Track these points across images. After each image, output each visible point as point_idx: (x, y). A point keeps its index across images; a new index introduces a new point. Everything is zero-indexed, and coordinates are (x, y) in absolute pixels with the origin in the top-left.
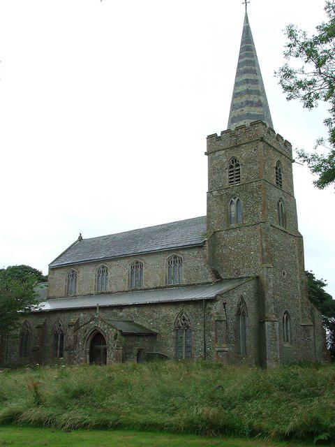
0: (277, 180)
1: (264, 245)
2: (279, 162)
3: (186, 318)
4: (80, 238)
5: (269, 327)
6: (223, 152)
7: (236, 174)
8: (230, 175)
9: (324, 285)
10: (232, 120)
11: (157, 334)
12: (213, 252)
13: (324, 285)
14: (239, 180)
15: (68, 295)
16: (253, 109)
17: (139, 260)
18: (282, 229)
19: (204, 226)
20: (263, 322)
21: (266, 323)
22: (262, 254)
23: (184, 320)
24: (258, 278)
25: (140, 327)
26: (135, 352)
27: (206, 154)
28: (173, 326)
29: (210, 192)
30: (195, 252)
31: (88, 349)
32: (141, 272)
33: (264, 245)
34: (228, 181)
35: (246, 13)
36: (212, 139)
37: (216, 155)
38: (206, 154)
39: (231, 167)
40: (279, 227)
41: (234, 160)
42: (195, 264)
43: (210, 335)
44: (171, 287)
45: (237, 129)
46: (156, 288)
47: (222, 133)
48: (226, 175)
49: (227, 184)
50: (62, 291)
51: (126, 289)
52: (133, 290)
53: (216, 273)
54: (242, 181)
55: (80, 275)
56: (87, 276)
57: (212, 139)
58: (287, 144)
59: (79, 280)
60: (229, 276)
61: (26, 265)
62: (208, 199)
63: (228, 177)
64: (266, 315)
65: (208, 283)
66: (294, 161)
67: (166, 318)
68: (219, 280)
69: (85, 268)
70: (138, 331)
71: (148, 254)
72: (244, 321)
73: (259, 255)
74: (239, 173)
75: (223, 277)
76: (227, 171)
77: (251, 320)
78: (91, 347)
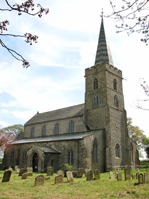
0: (114, 87)
1: (107, 115)
2: (115, 80)
3: (72, 147)
4: (38, 113)
5: (108, 150)
6: (91, 76)
7: (96, 85)
8: (94, 85)
9: (143, 132)
10: (96, 62)
11: (60, 153)
12: (86, 118)
13: (143, 132)
14: (97, 87)
15: (31, 137)
16: (104, 57)
17: (58, 122)
18: (116, 108)
19: (84, 107)
20: (106, 148)
21: (107, 149)
22: (106, 119)
23: (71, 147)
24: (104, 129)
25: (55, 150)
26: (50, 160)
27: (85, 76)
28: (66, 150)
29: (86, 93)
30: (79, 118)
31: (32, 160)
32: (74, 125)
33: (107, 115)
34: (93, 88)
35: (13, 35)
36: (87, 70)
37: (89, 77)
38: (85, 76)
39: (95, 82)
40: (115, 107)
41: (96, 79)
42: (79, 124)
43: (80, 154)
44: (70, 133)
45: (97, 66)
46: (64, 134)
47: (91, 67)
48: (93, 85)
49: (93, 89)
50: (29, 136)
51: (53, 135)
52: (56, 135)
53: (88, 128)
54: (98, 88)
55: (36, 128)
56: (38, 129)
57: (87, 70)
58: (120, 72)
59: (35, 130)
60: (93, 129)
61: (17, 124)
62: (85, 96)
63: (93, 86)
64: (107, 145)
65: (84, 132)
66: (123, 79)
67: (64, 147)
68: (89, 130)
69: (38, 125)
70: (55, 152)
71: (61, 119)
72: (97, 148)
73: (105, 119)
74: (97, 84)
75: (91, 129)
76: (93, 83)
77: (100, 147)
78: (33, 159)
